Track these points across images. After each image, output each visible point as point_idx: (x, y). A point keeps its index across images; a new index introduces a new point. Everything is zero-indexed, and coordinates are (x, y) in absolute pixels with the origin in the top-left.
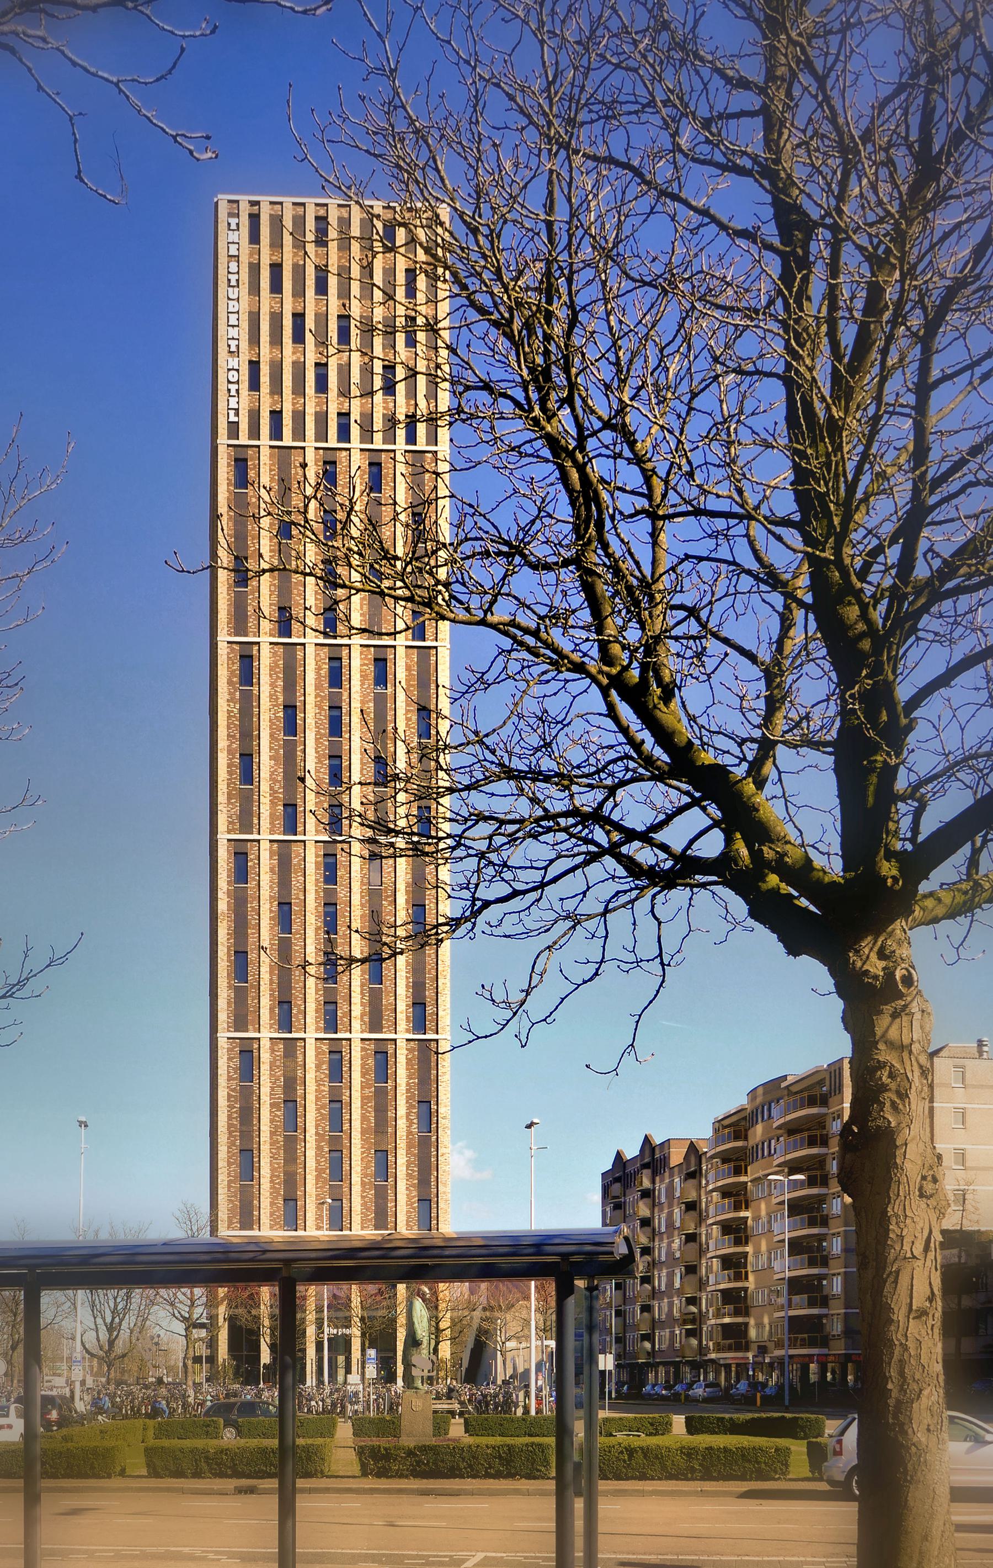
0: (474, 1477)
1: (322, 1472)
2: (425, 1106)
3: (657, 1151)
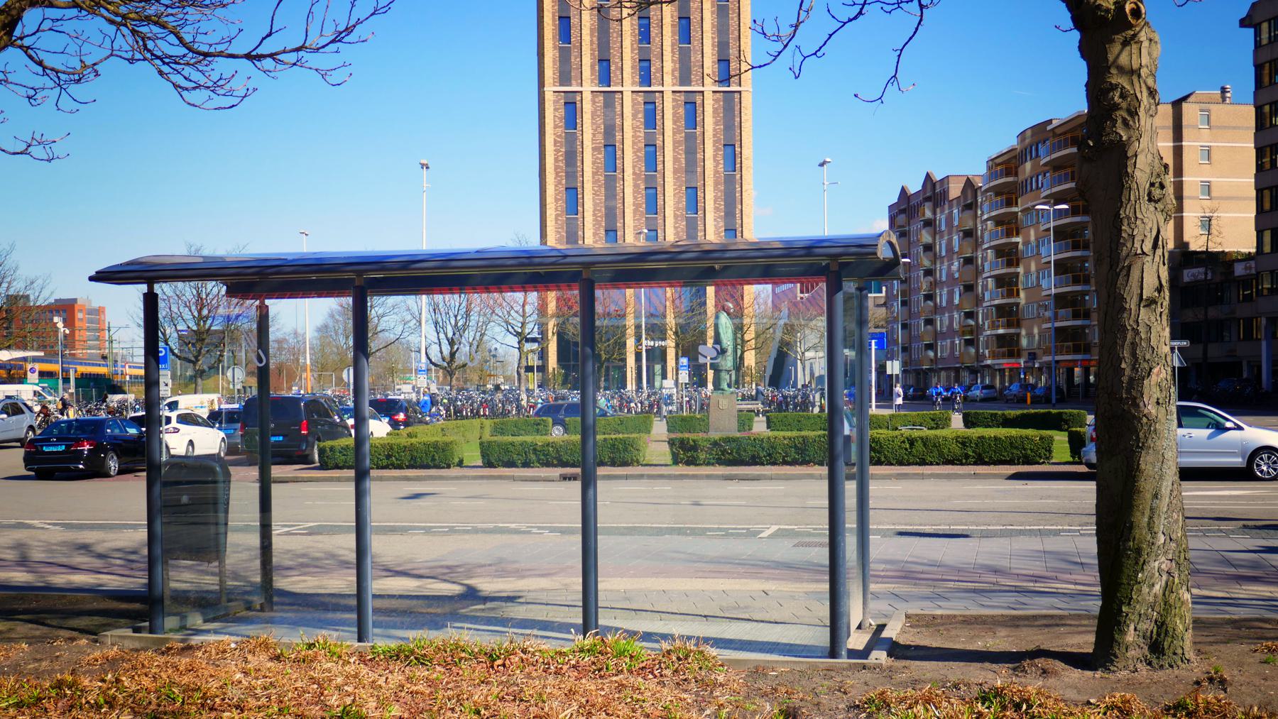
0: (774, 464)
1: (638, 462)
2: (729, 149)
3: (938, 186)
